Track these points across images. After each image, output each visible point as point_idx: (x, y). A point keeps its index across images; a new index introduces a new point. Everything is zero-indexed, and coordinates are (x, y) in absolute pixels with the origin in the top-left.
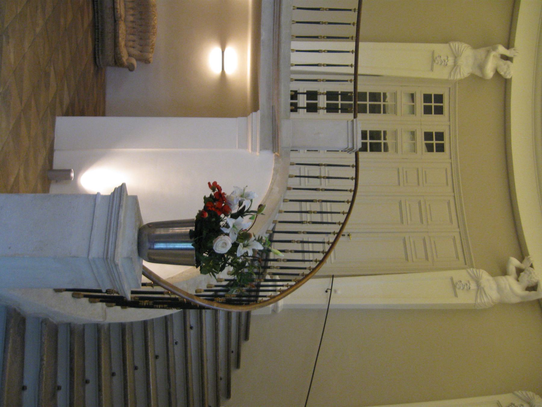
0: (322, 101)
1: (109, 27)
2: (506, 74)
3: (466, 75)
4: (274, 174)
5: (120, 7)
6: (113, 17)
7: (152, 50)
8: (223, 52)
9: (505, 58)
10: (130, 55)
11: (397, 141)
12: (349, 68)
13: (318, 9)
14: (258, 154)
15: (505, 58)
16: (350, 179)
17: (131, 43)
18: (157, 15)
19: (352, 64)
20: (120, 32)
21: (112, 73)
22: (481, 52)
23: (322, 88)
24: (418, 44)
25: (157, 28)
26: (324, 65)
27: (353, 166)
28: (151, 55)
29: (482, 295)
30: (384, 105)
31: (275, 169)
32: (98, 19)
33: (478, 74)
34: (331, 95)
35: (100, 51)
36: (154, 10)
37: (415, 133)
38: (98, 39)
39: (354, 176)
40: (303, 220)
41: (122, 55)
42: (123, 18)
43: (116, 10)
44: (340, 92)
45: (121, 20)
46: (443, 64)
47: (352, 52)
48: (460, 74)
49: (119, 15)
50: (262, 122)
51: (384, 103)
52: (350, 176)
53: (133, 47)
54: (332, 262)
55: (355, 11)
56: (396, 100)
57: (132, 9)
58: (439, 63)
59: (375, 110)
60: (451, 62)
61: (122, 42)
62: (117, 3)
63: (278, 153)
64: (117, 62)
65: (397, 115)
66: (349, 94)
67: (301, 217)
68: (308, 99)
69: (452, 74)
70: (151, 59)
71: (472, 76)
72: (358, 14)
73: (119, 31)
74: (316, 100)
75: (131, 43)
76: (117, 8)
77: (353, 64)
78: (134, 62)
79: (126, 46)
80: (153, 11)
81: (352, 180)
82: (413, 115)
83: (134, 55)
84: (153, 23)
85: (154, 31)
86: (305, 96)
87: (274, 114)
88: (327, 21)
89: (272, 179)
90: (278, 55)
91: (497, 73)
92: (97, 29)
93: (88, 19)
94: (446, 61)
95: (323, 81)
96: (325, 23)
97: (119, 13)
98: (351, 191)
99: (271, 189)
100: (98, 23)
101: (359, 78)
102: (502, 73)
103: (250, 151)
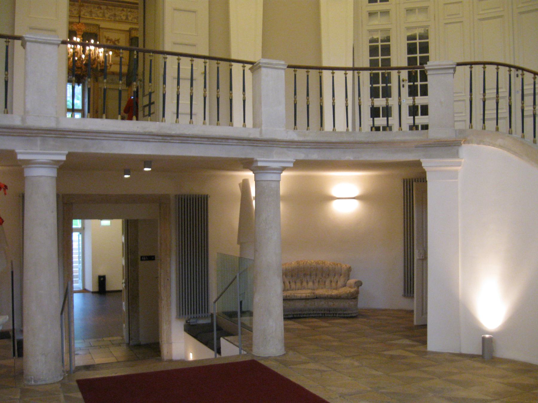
0: (380, 102)
1: (323, 304)
4: (485, 145)
6: (314, 300)
7: (339, 265)
8: (354, 198)
10: (345, 285)
11: (379, 29)
12: (348, 76)
14: (463, 161)
17: (334, 284)
18: (307, 260)
21: (362, 303)
23: (367, 103)
26: (347, 101)
27: (471, 68)
28: (344, 266)
30: (382, 41)
31: (478, 144)
32: (316, 314)
34: (374, 93)
35: (345, 312)
36: (302, 263)
37: (381, 11)
38: (334, 314)
39: (482, 66)
40: (532, 113)
41: (348, 292)
43: (308, 297)
44: (371, 86)
50: (430, 157)
51: (418, 38)
52: (482, 70)
53: (337, 282)
54: (464, 95)
55: (9, 42)
56: (377, 31)
57: (302, 283)
59: (386, 50)
61: (334, 293)
62: (301, 296)
63: (462, 140)
64: (354, 297)
65: (391, 29)
66: (372, 75)
67: (528, 116)
68: (379, 116)
70: (347, 266)
74: (379, 108)
75: (334, 284)
76: (306, 296)
78: (352, 281)
79: (336, 289)
80: (303, 263)
81: (472, 67)
82: (390, 12)
83: (344, 282)
84: (314, 264)
86: (375, 119)
87: (423, 146)
89: (489, 145)
90: (367, 143)
96: (295, 98)
97: (309, 295)
98: (498, 69)
99: (500, 146)
100: (319, 314)
101: (356, 66)
103: (459, 168)
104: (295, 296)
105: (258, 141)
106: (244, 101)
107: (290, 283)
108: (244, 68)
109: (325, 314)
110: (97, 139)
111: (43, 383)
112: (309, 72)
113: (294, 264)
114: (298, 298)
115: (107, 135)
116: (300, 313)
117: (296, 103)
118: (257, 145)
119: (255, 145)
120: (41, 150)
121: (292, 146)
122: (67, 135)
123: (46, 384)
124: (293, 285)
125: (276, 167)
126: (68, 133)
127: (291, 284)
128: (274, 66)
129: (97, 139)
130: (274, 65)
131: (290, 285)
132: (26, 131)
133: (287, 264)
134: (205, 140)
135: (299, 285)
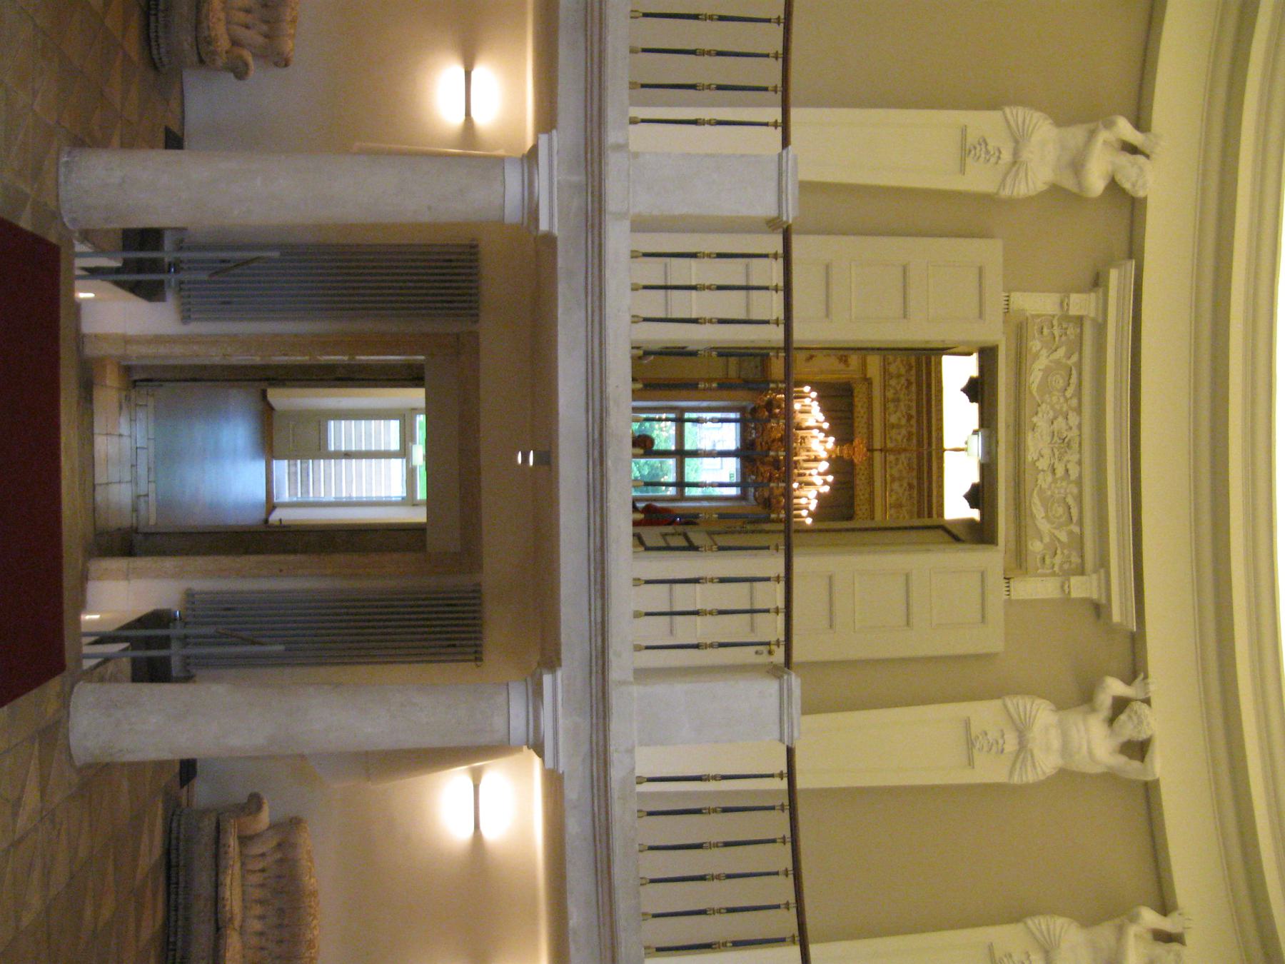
2: (1137, 188)
3: (1041, 187)
5: (231, 896)
9: (1132, 149)
12: (772, 327)
13: (699, 846)
15: (1132, 149)
16: (771, 126)
19: (776, 121)
20: (228, 955)
22: (1076, 134)
24: (938, 781)
25: (318, 947)
26: (715, 778)
29: (1026, 771)
33: (1069, 183)
36: (313, 903)
42: (237, 923)
43: (220, 905)
45: (231, 926)
46: (994, 748)
47: (778, 21)
48: (1027, 183)
49: (228, 915)
55: (784, 843)
57: (260, 902)
58: (986, 749)
60: (1011, 744)
62: (225, 885)
69: (1009, 181)
71: (1055, 191)
72: (790, 814)
73: (225, 953)
76: (223, 898)
77: (780, 251)
80: (310, 907)
84: (309, 936)
85: (312, 955)
88: (722, 872)
91: (1113, 186)
92: (172, 950)
93: (152, 923)
94: (1001, 741)
95: (710, 123)
96: (718, 877)
97: (228, 908)
102: (1127, 186)
104: (226, 868)
105: (603, 673)
106: (697, 646)
107: (263, 870)
108: (777, 808)
109: (175, 950)
110: (586, 296)
111: (62, 179)
112: (782, 779)
113: (310, 882)
114: (221, 877)
115: (597, 318)
116: (182, 885)
117: (702, 813)
118: (594, 674)
119: (594, 669)
120: (558, 183)
121: (595, 766)
122: (593, 234)
123: (57, 184)
124: (255, 879)
125: (542, 722)
126: (596, 233)
127: (259, 874)
128: (785, 711)
129: (586, 296)
130: (788, 710)
131: (255, 871)
132: (596, 154)
133: (309, 864)
134: (598, 539)
135: (258, 893)
